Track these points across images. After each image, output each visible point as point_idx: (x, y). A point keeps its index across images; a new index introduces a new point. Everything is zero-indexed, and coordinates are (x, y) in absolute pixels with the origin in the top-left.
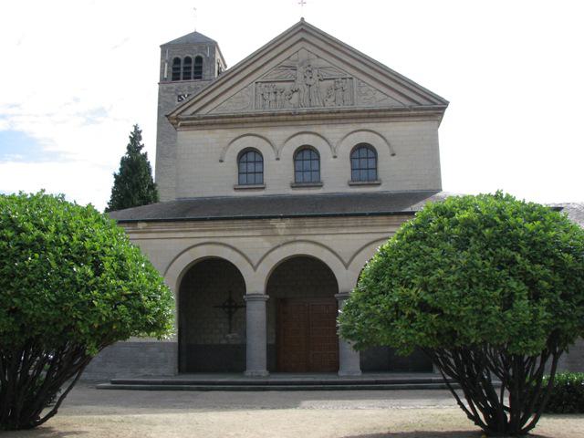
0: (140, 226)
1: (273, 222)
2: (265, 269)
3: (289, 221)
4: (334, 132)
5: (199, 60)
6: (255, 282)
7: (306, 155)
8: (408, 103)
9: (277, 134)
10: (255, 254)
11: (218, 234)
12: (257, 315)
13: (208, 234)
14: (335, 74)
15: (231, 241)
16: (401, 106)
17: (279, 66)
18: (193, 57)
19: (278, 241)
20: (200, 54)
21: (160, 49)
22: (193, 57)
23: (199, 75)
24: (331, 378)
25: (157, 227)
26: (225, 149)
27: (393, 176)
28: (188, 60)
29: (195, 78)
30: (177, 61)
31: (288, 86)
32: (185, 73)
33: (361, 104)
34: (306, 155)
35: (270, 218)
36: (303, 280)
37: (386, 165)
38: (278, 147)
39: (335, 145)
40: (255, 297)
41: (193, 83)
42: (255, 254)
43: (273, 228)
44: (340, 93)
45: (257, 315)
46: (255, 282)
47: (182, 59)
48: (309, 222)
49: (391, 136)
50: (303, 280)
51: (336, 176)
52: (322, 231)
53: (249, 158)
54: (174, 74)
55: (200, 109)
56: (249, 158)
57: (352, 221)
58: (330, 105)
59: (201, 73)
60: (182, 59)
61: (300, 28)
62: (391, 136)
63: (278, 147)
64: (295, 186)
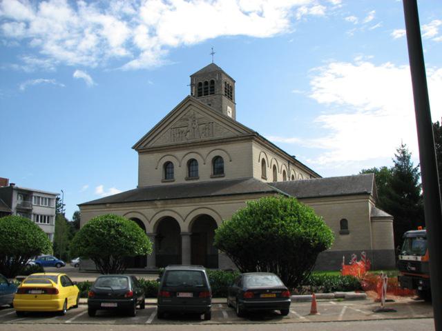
0: (108, 205)
1: (155, 202)
2: (153, 223)
3: (162, 202)
4: (204, 151)
5: (213, 82)
6: (184, 227)
7: (192, 163)
8: (237, 133)
9: (180, 154)
10: (184, 214)
11: (136, 208)
12: (186, 242)
13: (133, 208)
14: (205, 121)
15: (141, 211)
16: (235, 135)
17: (180, 119)
18: (209, 81)
19: (158, 210)
20: (213, 79)
21: (190, 78)
22: (209, 81)
23: (213, 92)
24: (143, 270)
25: (113, 206)
26: (158, 163)
27: (231, 172)
28: (206, 83)
29: (211, 94)
30: (200, 84)
31: (185, 129)
32: (205, 92)
33: (217, 136)
34: (192, 163)
35: (154, 200)
36: (204, 224)
37: (227, 166)
38: (180, 160)
39: (204, 158)
40: (185, 234)
41: (210, 97)
42: (184, 214)
43: (156, 205)
44: (207, 131)
45: (186, 242)
46: (184, 227)
47: (203, 82)
48: (169, 201)
49: (230, 152)
50: (204, 224)
51: (205, 173)
52: (176, 205)
53: (168, 166)
54: (199, 93)
55: (148, 143)
56: (168, 166)
57: (186, 201)
58: (204, 138)
59: (214, 90)
60: (203, 82)
61: (188, 104)
62: (230, 152)
63: (180, 160)
64: (187, 179)
